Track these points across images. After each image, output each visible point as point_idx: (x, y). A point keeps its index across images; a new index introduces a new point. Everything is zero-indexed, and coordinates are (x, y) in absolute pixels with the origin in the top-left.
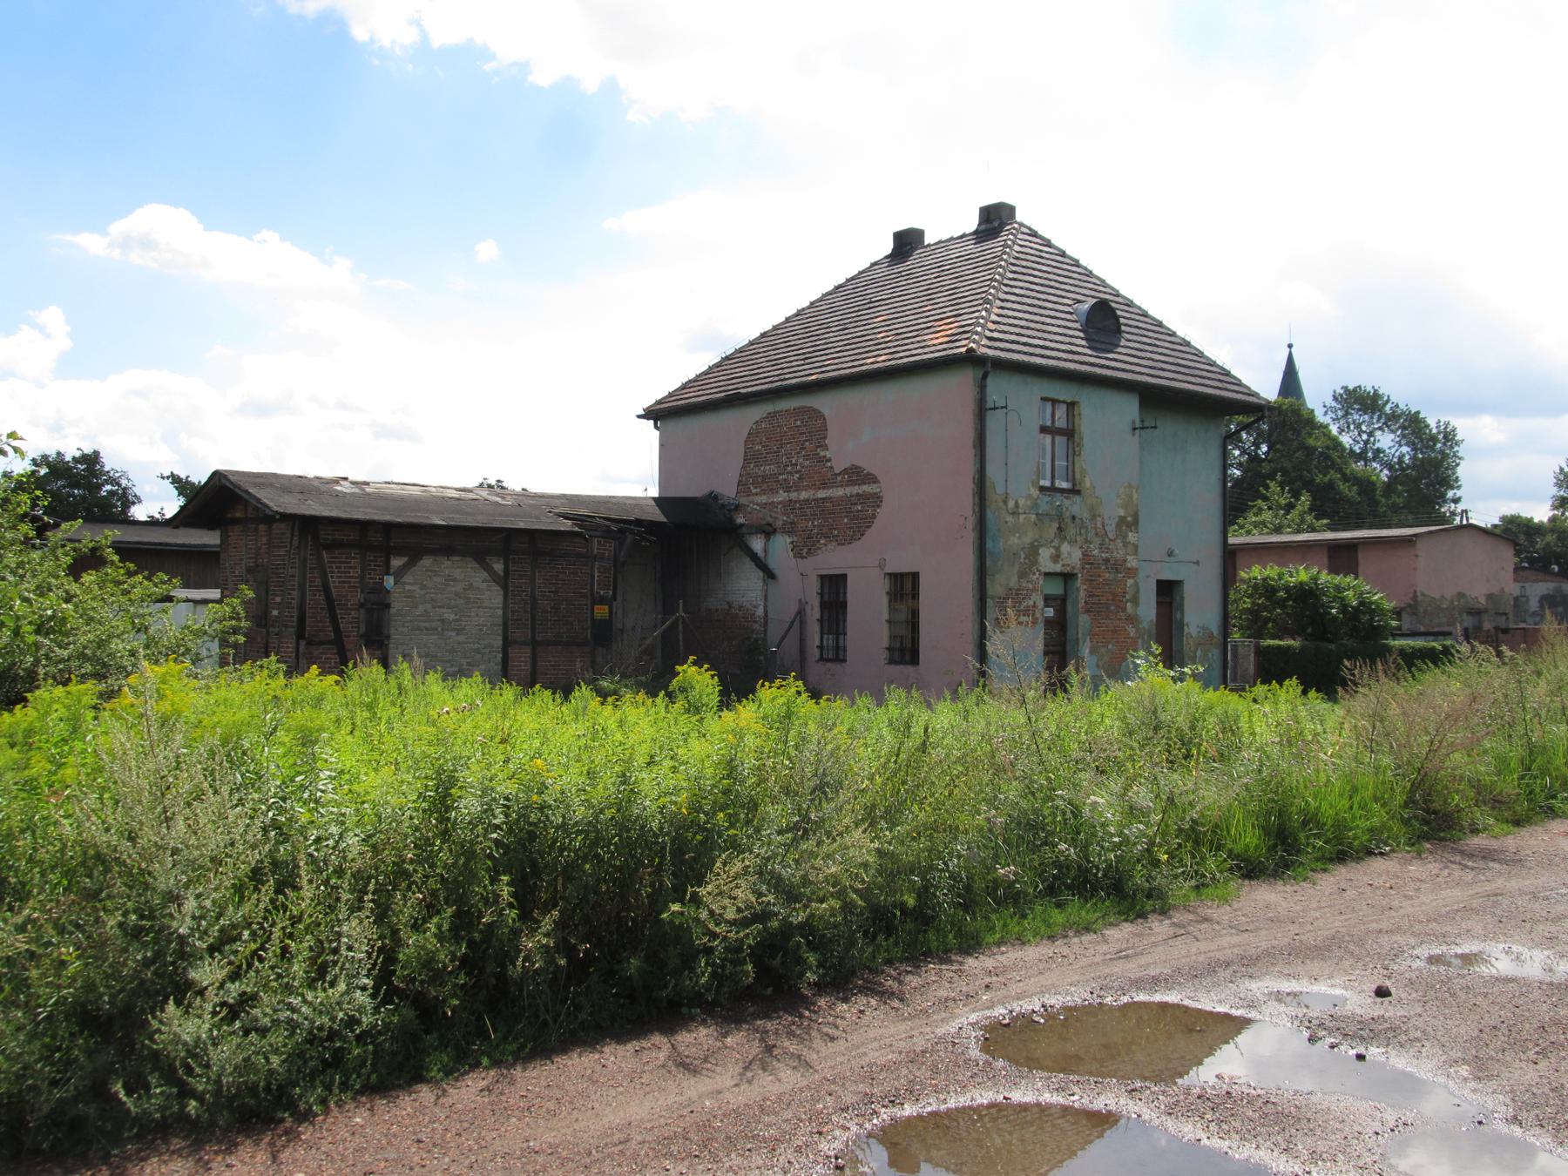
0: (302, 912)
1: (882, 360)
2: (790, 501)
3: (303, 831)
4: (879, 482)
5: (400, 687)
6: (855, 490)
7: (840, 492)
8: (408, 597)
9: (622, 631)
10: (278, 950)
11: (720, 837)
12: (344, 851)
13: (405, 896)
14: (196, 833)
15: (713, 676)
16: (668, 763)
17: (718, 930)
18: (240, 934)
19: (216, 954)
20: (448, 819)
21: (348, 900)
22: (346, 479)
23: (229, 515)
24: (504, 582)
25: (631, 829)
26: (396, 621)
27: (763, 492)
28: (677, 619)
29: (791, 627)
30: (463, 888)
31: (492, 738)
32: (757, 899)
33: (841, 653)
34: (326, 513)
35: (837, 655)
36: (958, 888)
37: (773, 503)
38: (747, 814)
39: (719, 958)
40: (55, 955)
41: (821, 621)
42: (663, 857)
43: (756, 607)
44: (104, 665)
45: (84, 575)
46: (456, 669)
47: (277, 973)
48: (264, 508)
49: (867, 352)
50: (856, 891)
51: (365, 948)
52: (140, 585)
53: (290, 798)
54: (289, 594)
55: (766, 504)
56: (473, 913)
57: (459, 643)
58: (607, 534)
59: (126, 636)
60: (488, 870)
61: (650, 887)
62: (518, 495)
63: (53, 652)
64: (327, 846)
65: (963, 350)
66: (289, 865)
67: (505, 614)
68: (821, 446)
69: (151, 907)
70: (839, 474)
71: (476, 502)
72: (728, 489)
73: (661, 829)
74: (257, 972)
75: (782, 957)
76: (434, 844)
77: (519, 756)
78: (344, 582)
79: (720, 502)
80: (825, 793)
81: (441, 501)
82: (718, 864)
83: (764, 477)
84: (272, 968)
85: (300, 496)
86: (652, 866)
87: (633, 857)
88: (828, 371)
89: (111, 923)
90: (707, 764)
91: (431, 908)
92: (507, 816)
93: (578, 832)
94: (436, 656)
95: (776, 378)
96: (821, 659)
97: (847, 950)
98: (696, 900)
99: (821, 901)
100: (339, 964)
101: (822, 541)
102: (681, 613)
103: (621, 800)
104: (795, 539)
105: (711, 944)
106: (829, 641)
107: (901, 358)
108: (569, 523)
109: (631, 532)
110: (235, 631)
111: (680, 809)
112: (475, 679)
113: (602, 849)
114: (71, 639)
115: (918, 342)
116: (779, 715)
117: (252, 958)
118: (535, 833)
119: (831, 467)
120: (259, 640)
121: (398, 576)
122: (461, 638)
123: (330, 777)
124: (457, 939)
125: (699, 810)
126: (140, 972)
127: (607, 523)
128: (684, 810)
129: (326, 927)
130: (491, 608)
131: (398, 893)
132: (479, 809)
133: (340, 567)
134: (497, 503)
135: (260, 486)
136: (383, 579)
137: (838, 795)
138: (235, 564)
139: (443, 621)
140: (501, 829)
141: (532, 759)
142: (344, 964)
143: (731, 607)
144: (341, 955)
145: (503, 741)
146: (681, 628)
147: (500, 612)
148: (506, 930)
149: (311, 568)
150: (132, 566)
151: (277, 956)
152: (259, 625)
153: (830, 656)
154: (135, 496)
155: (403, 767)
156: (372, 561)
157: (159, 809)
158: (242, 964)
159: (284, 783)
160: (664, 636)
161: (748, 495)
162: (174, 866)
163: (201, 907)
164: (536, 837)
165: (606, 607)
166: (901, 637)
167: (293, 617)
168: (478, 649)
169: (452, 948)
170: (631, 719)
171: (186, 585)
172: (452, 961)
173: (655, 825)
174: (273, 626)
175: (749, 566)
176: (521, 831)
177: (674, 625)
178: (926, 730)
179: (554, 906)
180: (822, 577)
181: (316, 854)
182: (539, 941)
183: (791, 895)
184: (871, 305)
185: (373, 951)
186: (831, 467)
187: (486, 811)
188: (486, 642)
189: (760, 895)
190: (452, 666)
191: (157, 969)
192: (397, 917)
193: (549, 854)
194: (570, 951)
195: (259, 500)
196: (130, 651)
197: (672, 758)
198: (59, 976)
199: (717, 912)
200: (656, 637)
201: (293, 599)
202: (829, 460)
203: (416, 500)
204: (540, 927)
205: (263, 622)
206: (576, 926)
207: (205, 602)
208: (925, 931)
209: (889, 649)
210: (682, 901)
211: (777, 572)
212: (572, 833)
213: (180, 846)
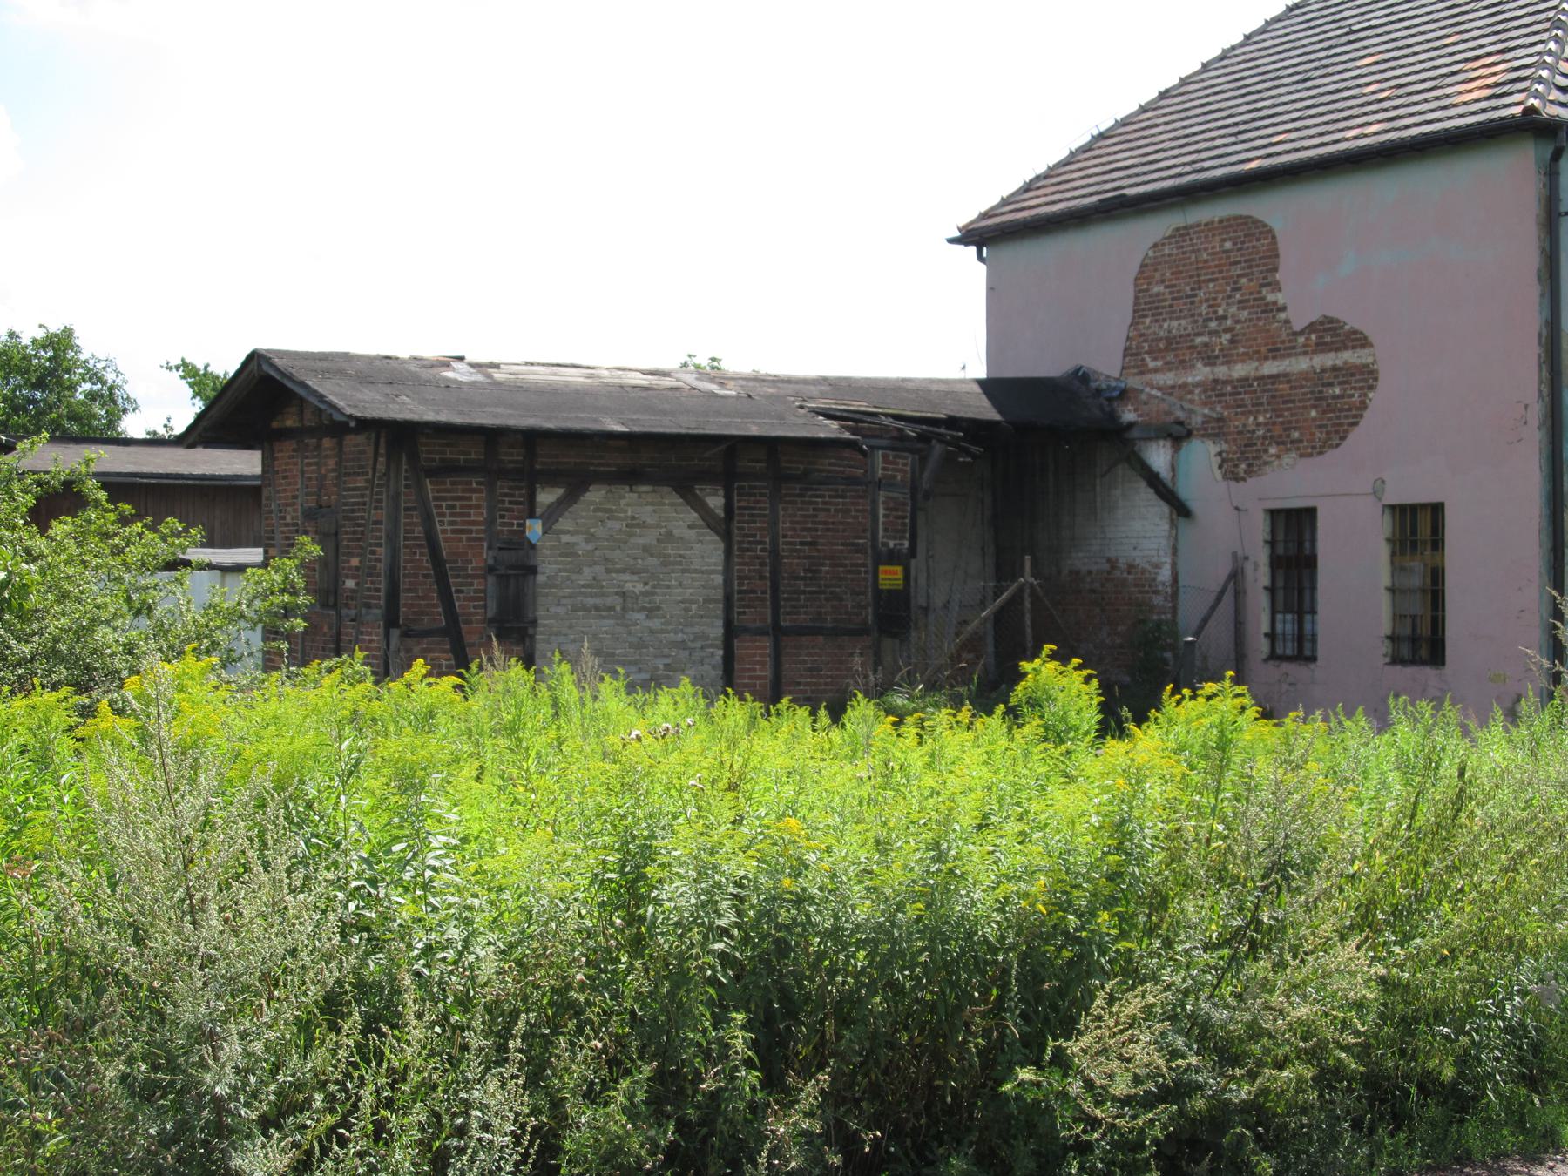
0: (406, 1067)
1: (1373, 132)
2: (1216, 381)
3: (405, 934)
4: (1371, 345)
5: (555, 704)
6: (1329, 360)
7: (1301, 364)
8: (567, 555)
9: (926, 610)
10: (370, 1127)
11: (1103, 953)
12: (471, 967)
13: (572, 1044)
14: (236, 933)
15: (1087, 680)
16: (1012, 828)
17: (1098, 1113)
18: (308, 1101)
19: (272, 1131)
20: (642, 919)
21: (481, 1049)
22: (461, 359)
23: (275, 425)
24: (724, 527)
25: (950, 938)
26: (546, 595)
27: (1168, 366)
28: (1021, 589)
29: (1219, 599)
30: (668, 1033)
31: (714, 782)
32: (1168, 1061)
33: (1307, 645)
34: (430, 416)
35: (1302, 650)
36: (1520, 1048)
37: (1185, 385)
38: (1149, 916)
39: (1102, 1161)
40: (26, 1122)
41: (1272, 590)
42: (1005, 988)
43: (1157, 566)
44: (87, 668)
45: (54, 523)
46: (647, 676)
47: (369, 1165)
48: (330, 411)
49: (1346, 119)
50: (1346, 1048)
51: (509, 1128)
52: (147, 541)
53: (383, 880)
54: (373, 552)
55: (1173, 387)
56: (686, 1075)
57: (652, 632)
58: (899, 442)
59: (120, 622)
60: (710, 1003)
61: (983, 1037)
62: (747, 379)
63: (9, 648)
64: (444, 960)
65: (1517, 110)
66: (383, 989)
67: (727, 582)
68: (1269, 284)
69: (168, 1052)
70: (1302, 332)
71: (677, 394)
72: (1106, 363)
73: (1002, 938)
74: (337, 1160)
75: (1212, 1161)
76: (617, 960)
77: (760, 812)
78: (461, 532)
79: (1093, 385)
80: (1287, 878)
81: (620, 395)
82: (1099, 1001)
83: (1170, 340)
84: (361, 1155)
85: (388, 390)
86: (986, 1002)
87: (953, 985)
88: (1279, 154)
89: (111, 1074)
90: (1080, 828)
91: (616, 1066)
92: (739, 914)
93: (860, 944)
94: (613, 654)
95: (1188, 169)
96: (1273, 656)
97: (1324, 1151)
98: (1062, 1062)
99: (1280, 1066)
100: (469, 1151)
101: (1272, 451)
102: (1028, 578)
103: (934, 888)
104: (1225, 447)
105: (1085, 1137)
106: (1286, 624)
107: (1407, 127)
108: (834, 424)
109: (941, 439)
110: (289, 611)
111: (1032, 905)
112: (682, 689)
113: (901, 971)
114: (35, 626)
115: (1437, 98)
116: (1204, 745)
117: (330, 1140)
118: (787, 943)
119: (1287, 321)
120: (326, 629)
121: (550, 517)
122: (656, 624)
123: (447, 846)
124: (660, 1117)
125: (1066, 906)
126: (156, 1153)
127: (900, 424)
128: (1041, 907)
129: (445, 1091)
130: (703, 572)
131: (561, 1038)
132: (693, 901)
133: (453, 507)
134: (712, 395)
135: (324, 373)
136: (524, 525)
137: (1310, 883)
138: (287, 505)
139: (623, 595)
140: (731, 937)
141: (780, 818)
142: (475, 1153)
143: (1113, 568)
144: (471, 1138)
145: (733, 787)
146: (1027, 604)
147: (719, 579)
148: (741, 1105)
149: (407, 509)
150: (127, 508)
151: (368, 1137)
152: (324, 605)
153: (1289, 652)
154: (128, 398)
155: (565, 830)
156: (506, 495)
157: (180, 893)
158: (313, 1147)
159: (372, 854)
160: (999, 616)
161: (1142, 373)
162: (205, 984)
163: (248, 1054)
164: (789, 948)
165: (899, 569)
166: (1414, 617)
167: (378, 590)
168: (683, 641)
169: (652, 1133)
170: (952, 751)
171: (210, 543)
172: (652, 1153)
173: (991, 932)
174: (347, 605)
175: (1144, 495)
176: (763, 938)
177: (1016, 599)
178: (1462, 773)
179: (821, 1068)
180: (1274, 514)
181: (426, 971)
182: (795, 1124)
183: (1226, 1054)
184: (1352, 37)
185: (524, 1133)
186: (1287, 321)
187: (704, 905)
188: (696, 629)
189: (1174, 1054)
190: (640, 671)
191: (181, 1151)
192: (561, 1078)
193: (811, 980)
194: (847, 1142)
195: (321, 398)
196: (124, 645)
197: (1020, 819)
198: (31, 1156)
199: (1098, 1082)
200: (986, 619)
201: (378, 560)
202: (1283, 309)
203: (577, 392)
204: (797, 1102)
205: (331, 600)
206: (857, 1102)
207: (239, 569)
208: (1462, 1121)
209: (1393, 638)
210: (1037, 1064)
211: (1194, 505)
212: (850, 945)
213: (213, 952)
